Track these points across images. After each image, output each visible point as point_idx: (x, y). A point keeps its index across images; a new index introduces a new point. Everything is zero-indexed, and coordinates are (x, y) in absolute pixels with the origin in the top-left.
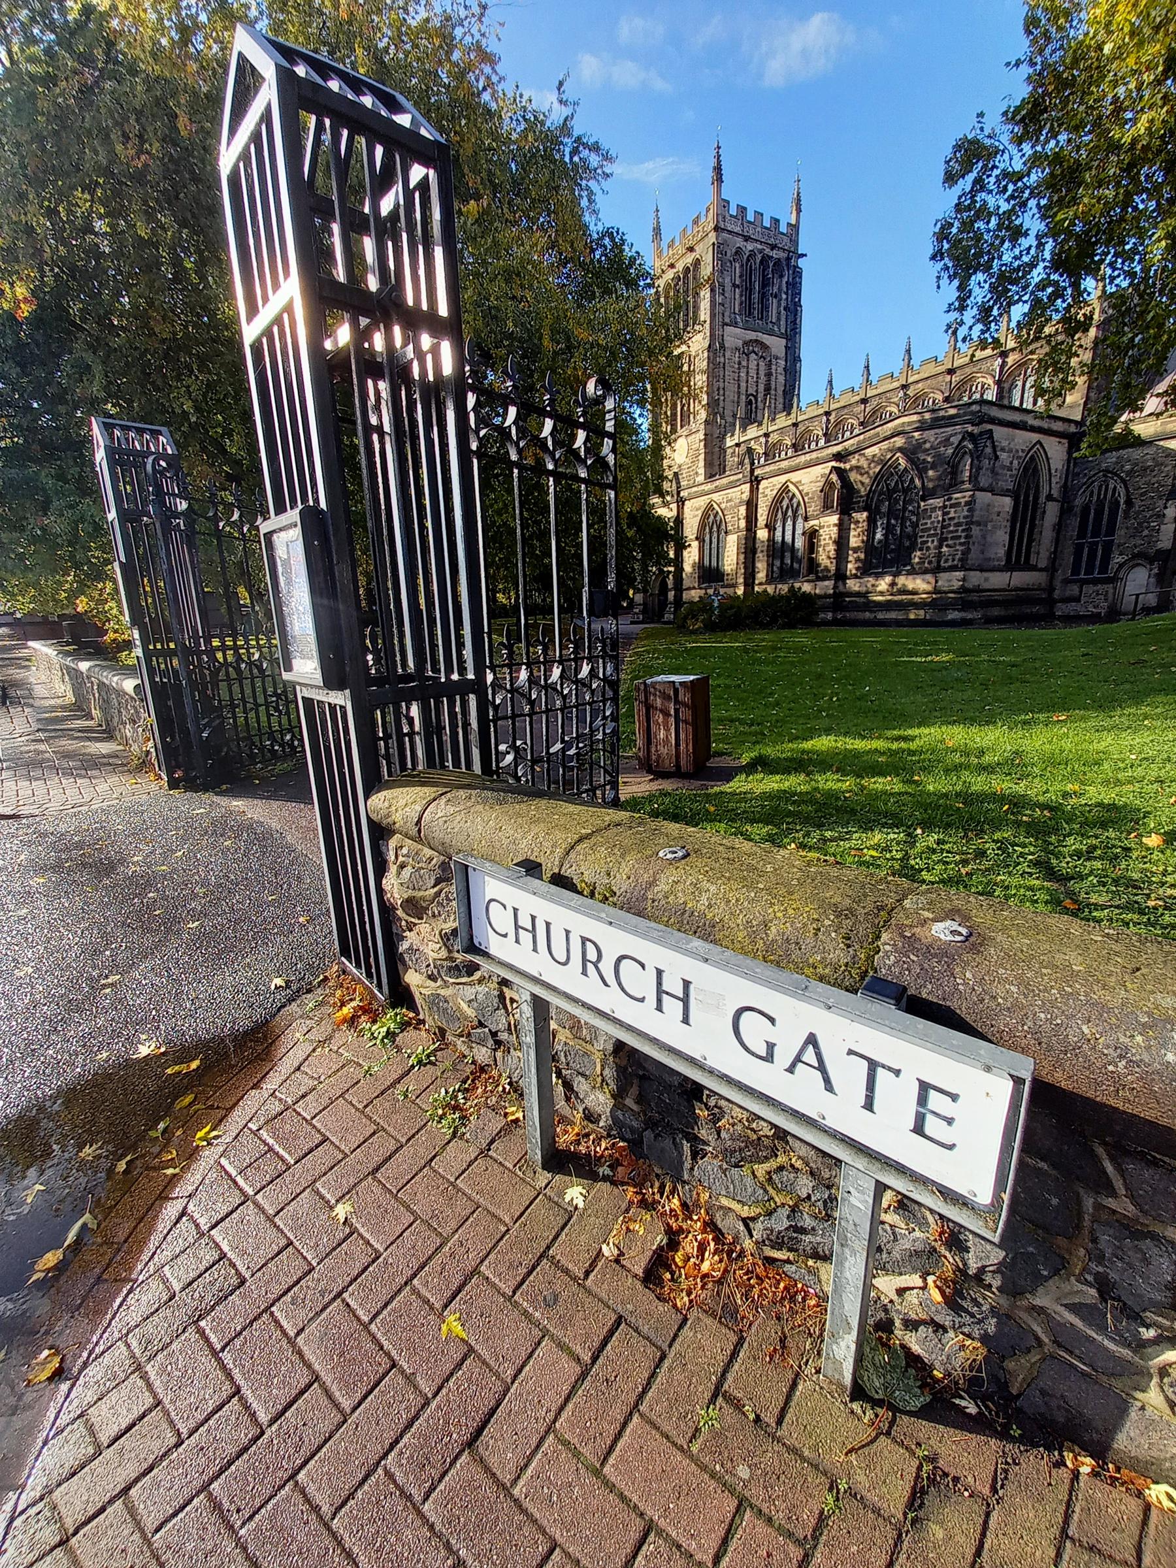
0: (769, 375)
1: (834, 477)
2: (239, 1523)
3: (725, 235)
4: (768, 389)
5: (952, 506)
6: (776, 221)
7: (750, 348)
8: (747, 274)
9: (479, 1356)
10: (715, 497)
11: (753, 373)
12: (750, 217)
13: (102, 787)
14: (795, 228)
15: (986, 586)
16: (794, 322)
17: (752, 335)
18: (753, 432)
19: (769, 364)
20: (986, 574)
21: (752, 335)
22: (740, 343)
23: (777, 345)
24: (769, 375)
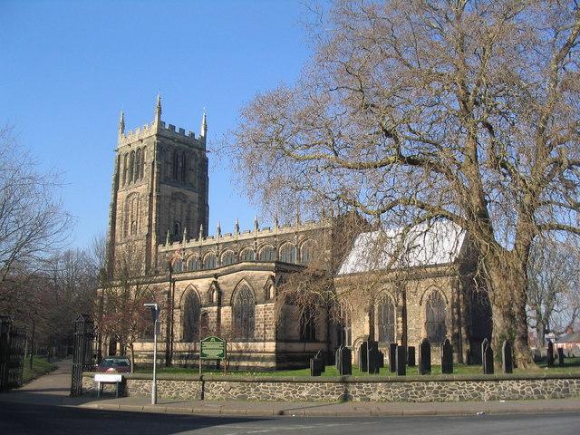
0: (189, 212)
1: (214, 286)
2: (161, 388)
3: (162, 139)
4: (188, 219)
5: (268, 309)
6: (193, 135)
7: (174, 197)
8: (175, 157)
9: (296, 341)
10: (195, 282)
11: (178, 210)
12: (177, 131)
13: (190, 409)
14: (204, 139)
15: (289, 349)
16: (204, 185)
17: (177, 190)
18: (176, 246)
19: (189, 206)
20: (291, 344)
21: (177, 190)
22: (170, 194)
23: (193, 196)
24: (189, 212)
